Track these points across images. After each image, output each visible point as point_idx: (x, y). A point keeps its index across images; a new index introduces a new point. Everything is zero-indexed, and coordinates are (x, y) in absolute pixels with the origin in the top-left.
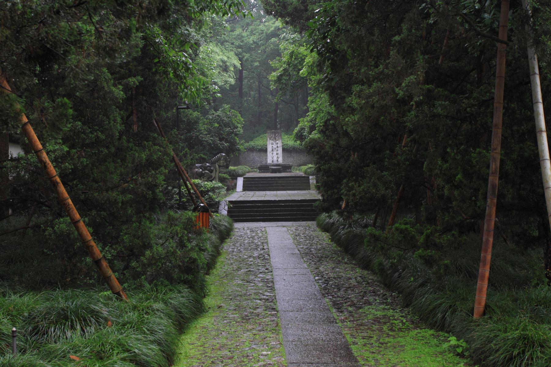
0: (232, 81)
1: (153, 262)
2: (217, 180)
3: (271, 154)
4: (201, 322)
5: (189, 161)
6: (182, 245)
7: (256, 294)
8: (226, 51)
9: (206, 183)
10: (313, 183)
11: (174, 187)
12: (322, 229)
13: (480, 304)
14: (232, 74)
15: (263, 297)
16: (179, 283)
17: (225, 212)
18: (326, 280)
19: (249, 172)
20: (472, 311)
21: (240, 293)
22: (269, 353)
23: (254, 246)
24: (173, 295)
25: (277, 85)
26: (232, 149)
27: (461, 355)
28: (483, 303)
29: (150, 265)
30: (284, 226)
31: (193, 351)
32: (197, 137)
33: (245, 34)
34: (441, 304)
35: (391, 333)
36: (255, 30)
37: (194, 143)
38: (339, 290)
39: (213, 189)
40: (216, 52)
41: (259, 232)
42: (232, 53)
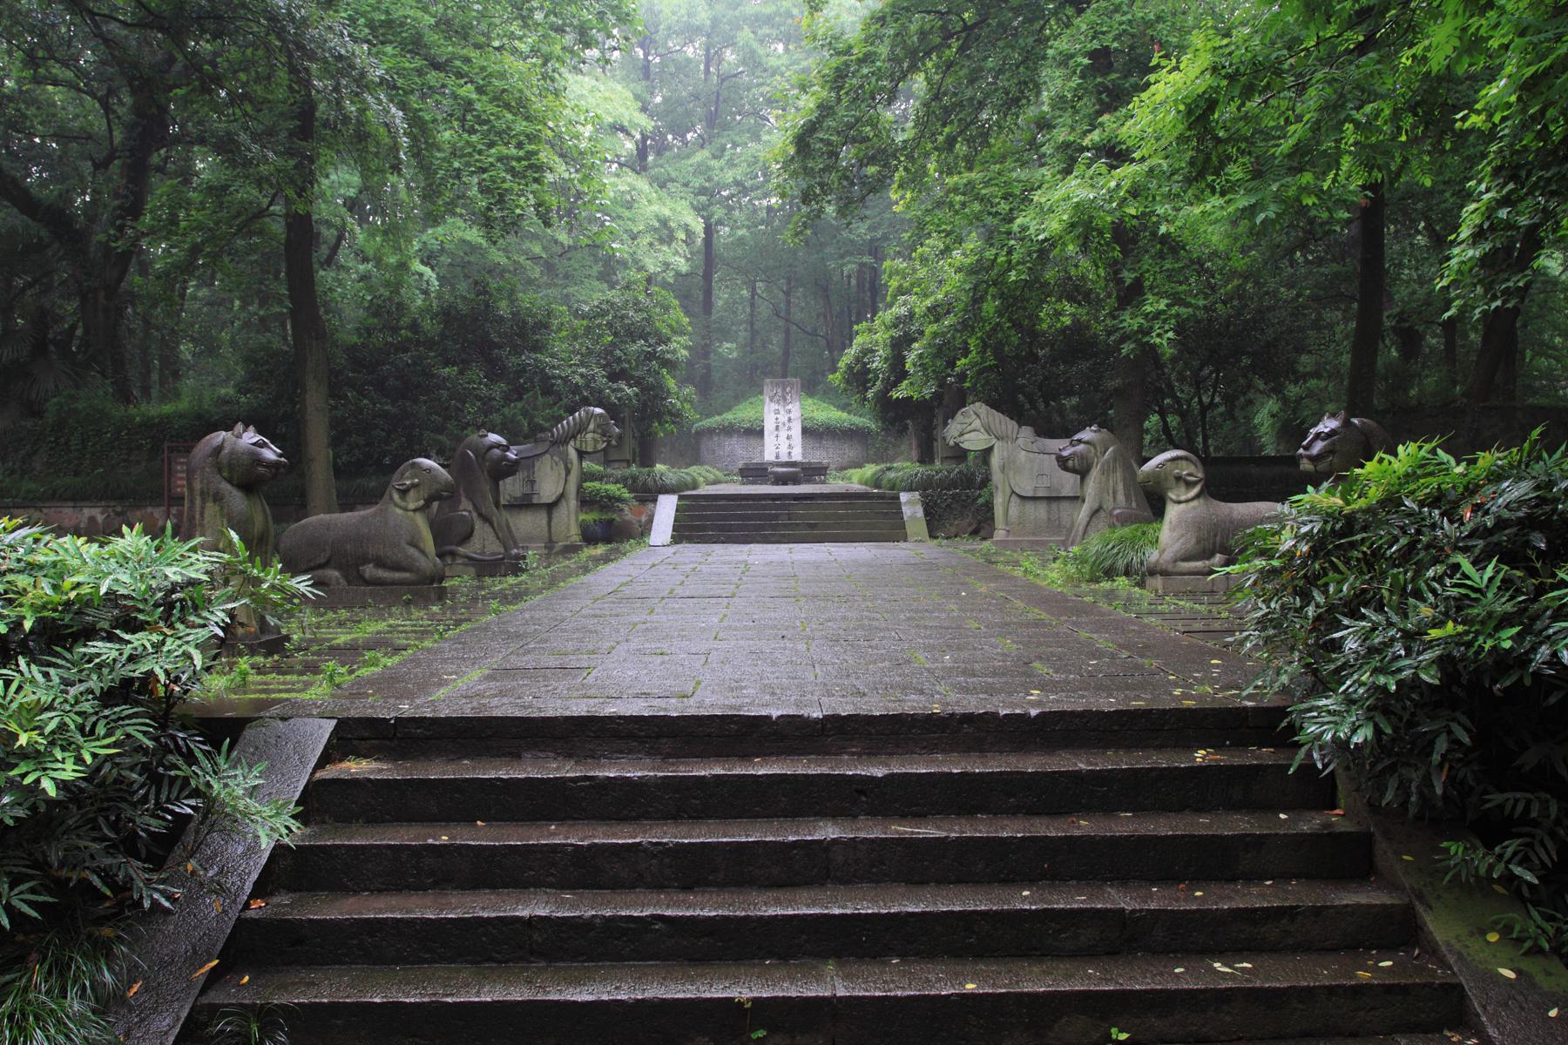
10: (913, 517)
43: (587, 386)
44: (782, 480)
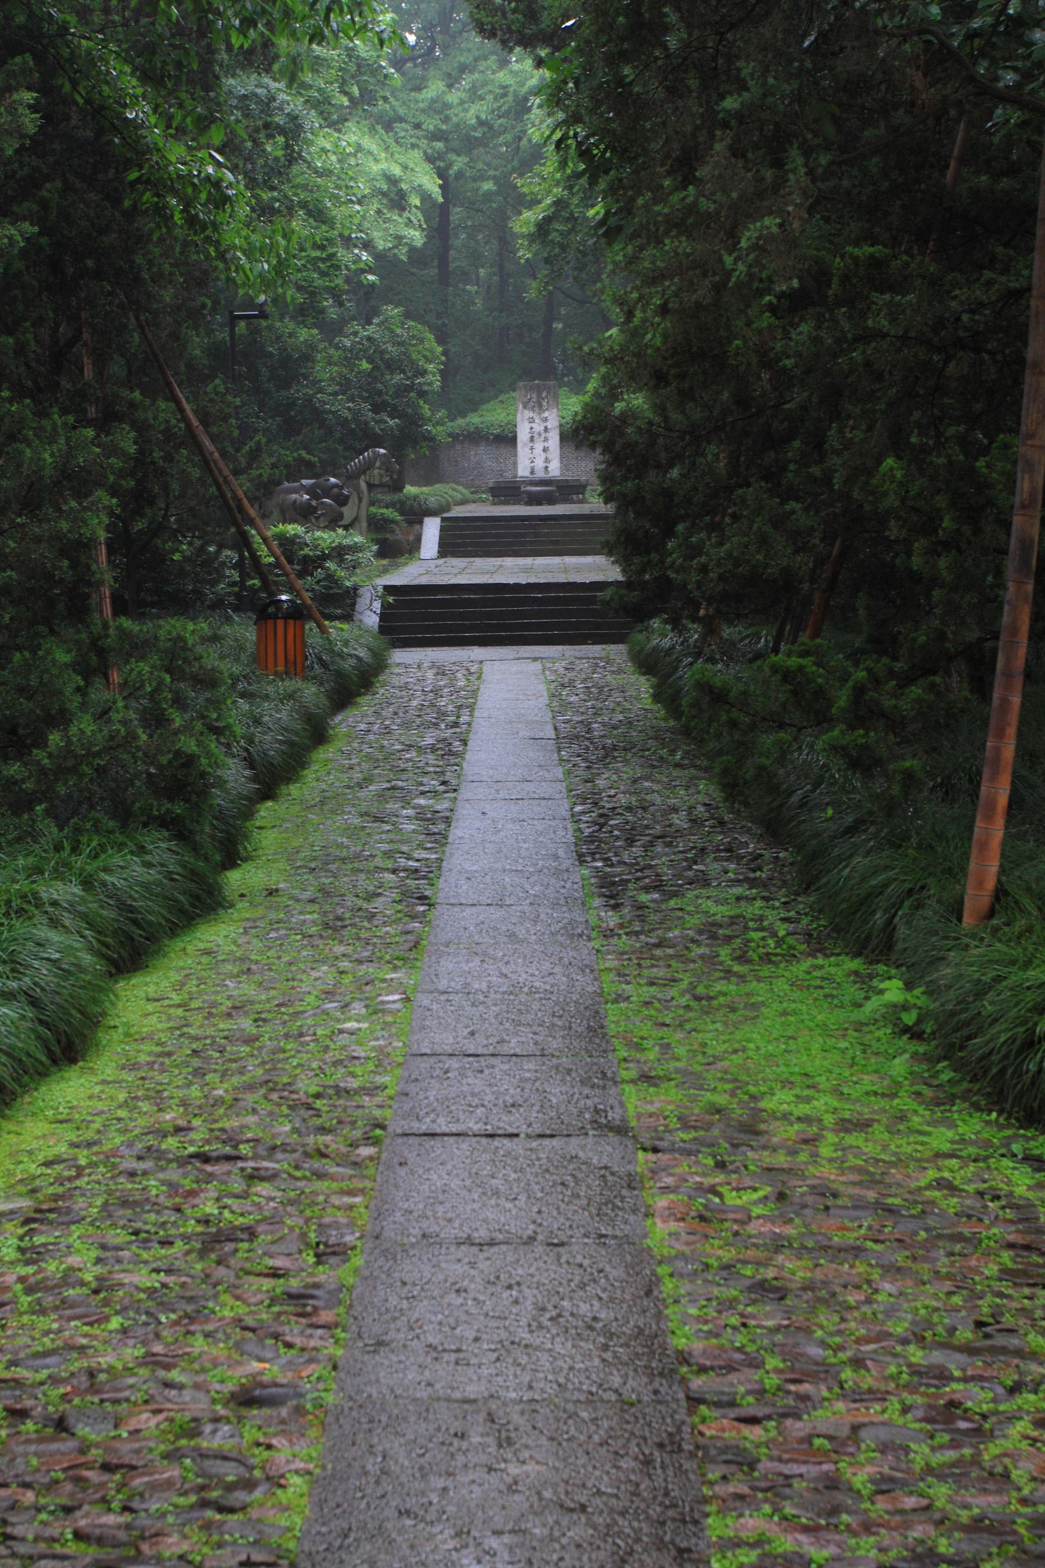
0: (416, 237)
1: (70, 763)
2: (364, 524)
3: (527, 450)
4: (206, 937)
5: (266, 472)
6: (155, 720)
7: (388, 855)
8: (397, 149)
9: (318, 534)
11: (221, 547)
12: (640, 666)
13: (980, 884)
14: (417, 216)
15: (403, 862)
16: (145, 825)
17: (371, 619)
18: (601, 816)
19: (463, 502)
20: (957, 910)
21: (345, 854)
22: (364, 1025)
23: (432, 716)
24: (117, 860)
25: (535, 247)
26: (409, 438)
27: (914, 1033)
28: (990, 884)
29: (61, 772)
30: (535, 659)
31: (153, 1019)
32: (309, 400)
33: (453, 98)
34: (886, 885)
35: (737, 968)
36: (485, 84)
37: (298, 420)
38: (630, 842)
39: (339, 553)
40: (370, 153)
41: (459, 675)
42: (416, 155)
43: (355, 419)
44: (535, 500)
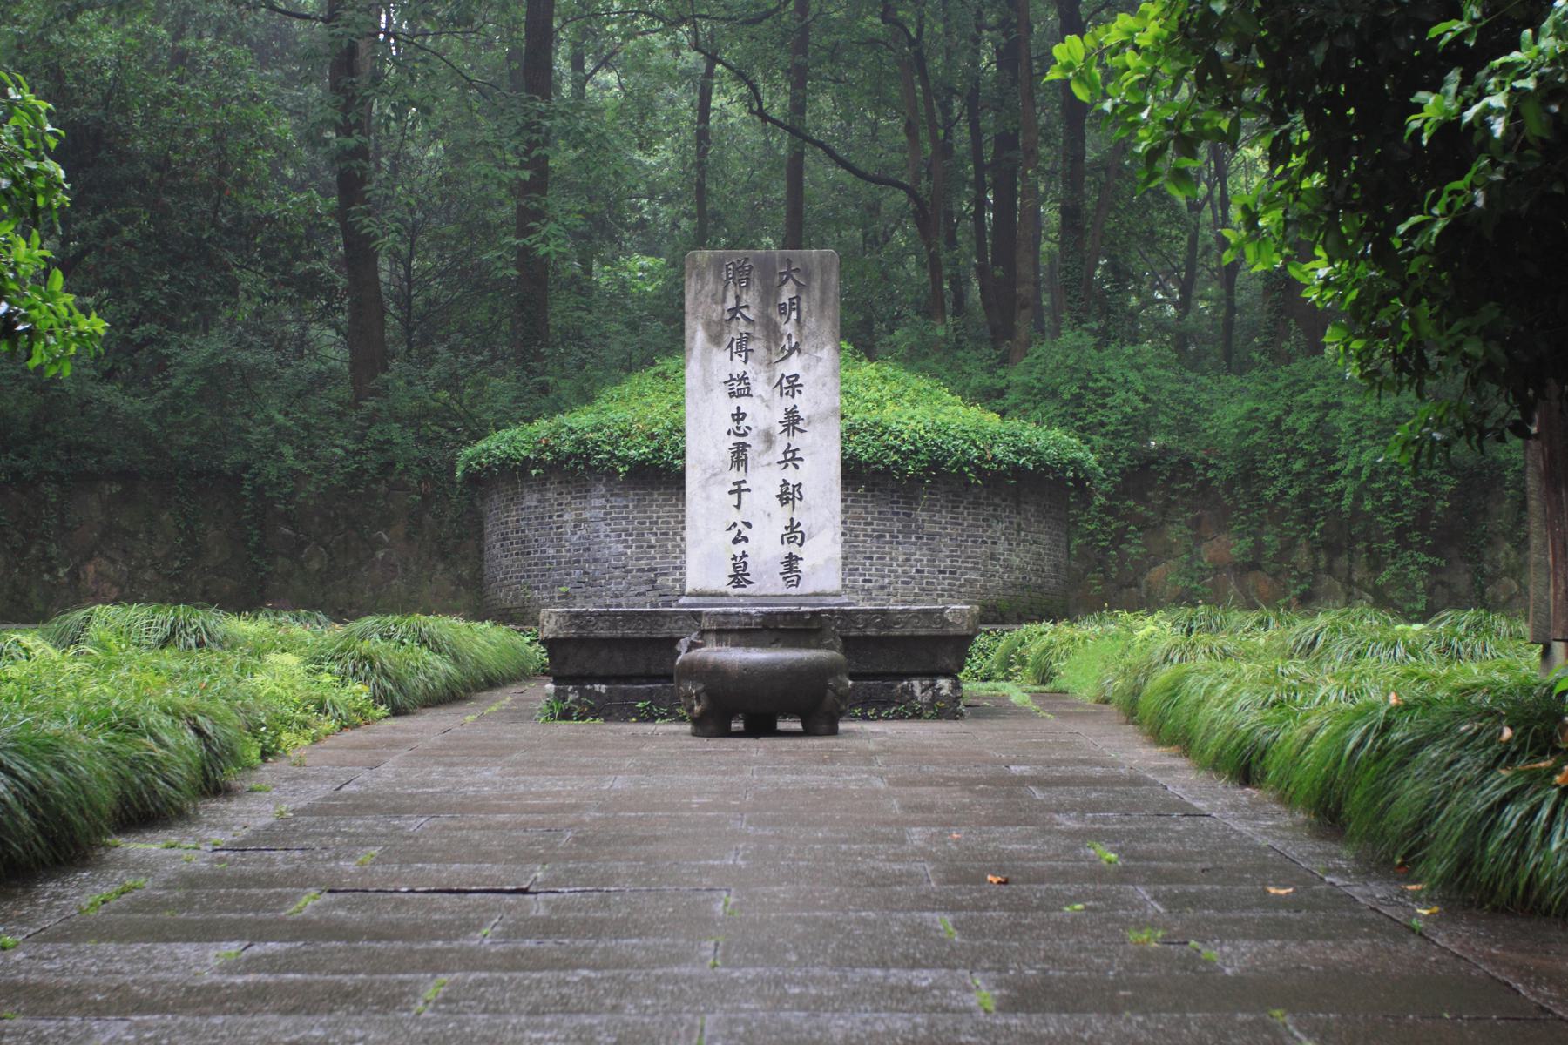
3: (721, 495)
